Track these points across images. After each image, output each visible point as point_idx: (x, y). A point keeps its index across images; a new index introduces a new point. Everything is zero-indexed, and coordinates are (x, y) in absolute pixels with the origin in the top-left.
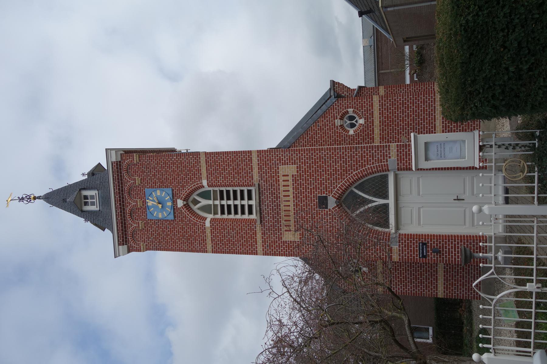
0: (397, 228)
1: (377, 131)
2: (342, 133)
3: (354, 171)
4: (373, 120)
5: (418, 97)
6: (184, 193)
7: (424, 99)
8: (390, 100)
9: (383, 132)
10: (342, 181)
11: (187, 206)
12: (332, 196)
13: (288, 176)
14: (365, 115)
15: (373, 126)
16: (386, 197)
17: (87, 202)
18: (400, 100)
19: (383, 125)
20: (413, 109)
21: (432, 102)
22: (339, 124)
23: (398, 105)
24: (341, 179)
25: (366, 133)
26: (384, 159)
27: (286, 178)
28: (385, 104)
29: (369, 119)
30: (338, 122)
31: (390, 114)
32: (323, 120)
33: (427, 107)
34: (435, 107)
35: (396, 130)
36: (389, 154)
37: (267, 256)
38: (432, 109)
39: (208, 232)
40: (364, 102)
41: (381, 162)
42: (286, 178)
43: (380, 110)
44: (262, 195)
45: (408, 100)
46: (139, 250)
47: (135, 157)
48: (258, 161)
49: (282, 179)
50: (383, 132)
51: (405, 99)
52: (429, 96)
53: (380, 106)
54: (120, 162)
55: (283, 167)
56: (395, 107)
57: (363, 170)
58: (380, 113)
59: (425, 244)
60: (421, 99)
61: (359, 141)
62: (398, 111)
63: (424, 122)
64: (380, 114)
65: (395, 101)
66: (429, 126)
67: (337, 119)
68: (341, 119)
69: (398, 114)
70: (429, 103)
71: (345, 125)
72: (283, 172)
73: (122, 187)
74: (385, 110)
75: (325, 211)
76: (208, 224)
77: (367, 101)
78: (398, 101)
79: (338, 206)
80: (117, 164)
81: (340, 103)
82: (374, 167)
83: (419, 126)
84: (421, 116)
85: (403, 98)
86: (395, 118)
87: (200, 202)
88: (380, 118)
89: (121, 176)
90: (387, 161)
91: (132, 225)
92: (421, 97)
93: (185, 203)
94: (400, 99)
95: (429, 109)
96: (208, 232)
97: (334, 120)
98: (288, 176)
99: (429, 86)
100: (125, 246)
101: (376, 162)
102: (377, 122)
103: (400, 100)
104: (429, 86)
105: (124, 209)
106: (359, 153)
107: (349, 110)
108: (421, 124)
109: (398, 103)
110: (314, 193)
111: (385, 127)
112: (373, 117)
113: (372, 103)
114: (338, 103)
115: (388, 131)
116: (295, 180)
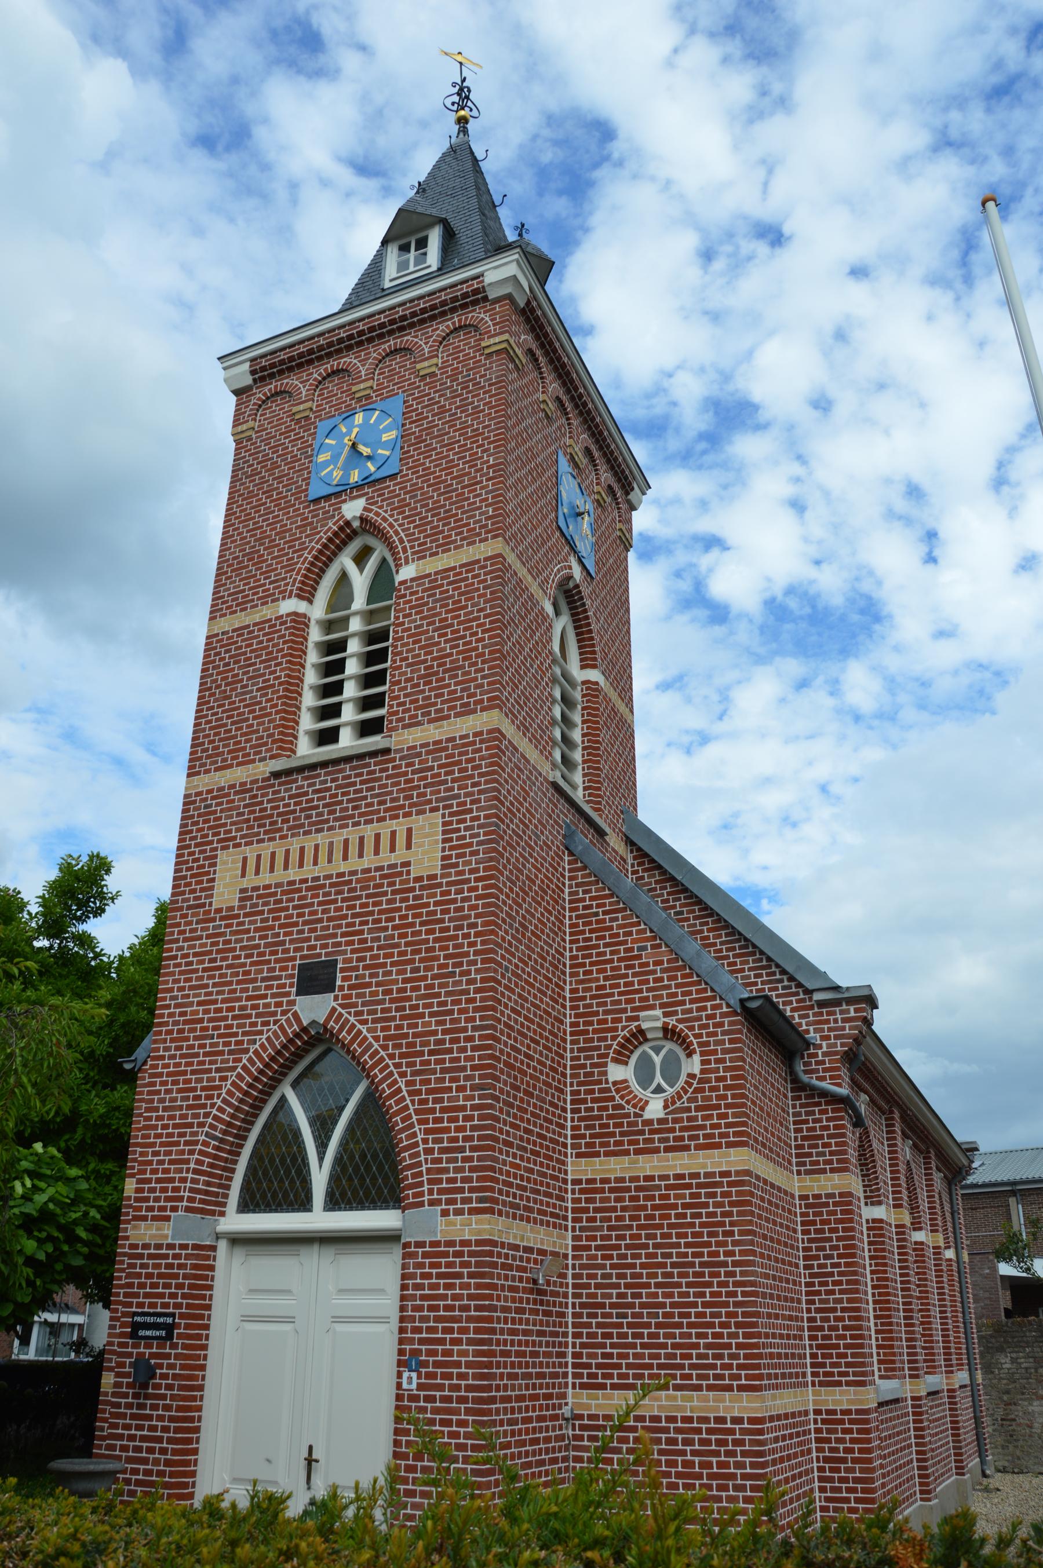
0: (238, 1240)
1: (616, 1167)
2: (614, 1038)
3: (408, 1084)
4: (657, 1151)
5: (738, 1325)
6: (385, 516)
7: (729, 1346)
8: (729, 1214)
9: (612, 1190)
10: (376, 1039)
11: (346, 534)
12: (334, 1010)
13: (409, 847)
14: (675, 1121)
15: (638, 1152)
16: (335, 1201)
17: (409, 251)
18: (727, 1254)
19: (638, 1189)
20: (694, 1305)
21: (717, 1377)
22: (645, 1026)
23: (708, 1244)
24: (386, 1038)
25: (613, 1126)
26: (441, 1191)
27: (401, 840)
28: (714, 1195)
29: (670, 1136)
30: (653, 1020)
31: (678, 1216)
32: (661, 963)
33: (699, 1356)
34: (698, 1388)
35: (618, 1238)
36: (459, 1212)
37: (180, 807)
38: (689, 1377)
39: (266, 612)
40: (724, 1116)
41: (430, 1182)
42: (401, 840)
43: (693, 1176)
44: (352, 769)
45: (725, 1284)
46: (236, 423)
47: (497, 340)
48: (462, 737)
49: (400, 826)
50: (612, 1190)
51: (732, 1274)
52: (740, 1367)
53: (707, 1175)
54: (485, 299)
55: (432, 825)
56: (700, 1235)
57: (409, 1117)
58: (681, 1177)
59: (169, 1336)
60: (731, 1336)
61: (585, 1101)
62: (688, 1245)
63: (644, 1346)
64: (678, 1177)
65: (726, 1234)
66: (629, 1366)
67: (665, 1015)
68: (665, 1029)
69: (678, 1245)
70: (714, 1367)
71: (646, 1048)
72: (423, 827)
73: (412, 325)
74: (693, 1196)
75: (291, 985)
76: (290, 605)
77: (728, 1125)
78: (724, 1244)
79: (305, 1030)
80: (476, 292)
81: (721, 1025)
82: (418, 1154)
83: (630, 1325)
84: (667, 1336)
85: (735, 1264)
86: (664, 1236)
87: (361, 570)
88: (662, 1178)
89: (443, 314)
90: (432, 1203)
91: (297, 383)
92: (735, 1335)
93: (356, 524)
94: (731, 1253)
95: (693, 1367)
96: (266, 612)
97: (662, 1006)
98: (409, 847)
99: (848, 1365)
100: (248, 380)
101: (436, 1161)
102: (648, 1165)
103: (727, 1254)
104: (848, 1365)
105: (349, 348)
106: (466, 1098)
107: (697, 1058)
108: (635, 1336)
109: (719, 1244)
110: (348, 943)
111: (632, 1199)
112: (667, 1150)
113: (718, 1146)
114: (724, 1015)
115: (614, 1209)
116: (392, 873)
